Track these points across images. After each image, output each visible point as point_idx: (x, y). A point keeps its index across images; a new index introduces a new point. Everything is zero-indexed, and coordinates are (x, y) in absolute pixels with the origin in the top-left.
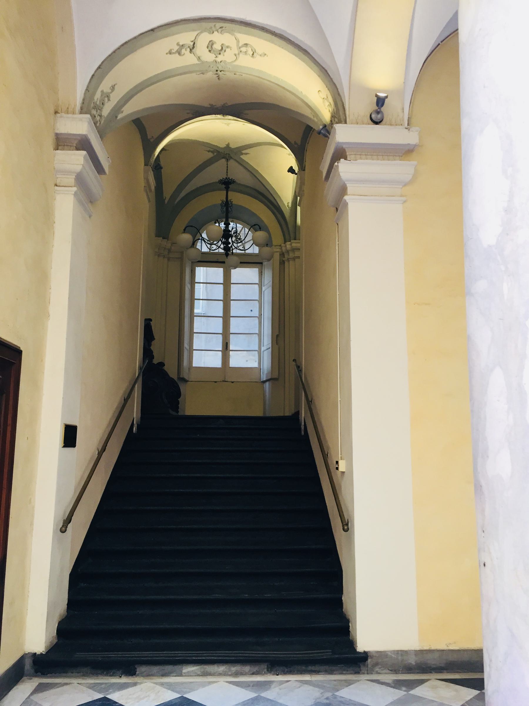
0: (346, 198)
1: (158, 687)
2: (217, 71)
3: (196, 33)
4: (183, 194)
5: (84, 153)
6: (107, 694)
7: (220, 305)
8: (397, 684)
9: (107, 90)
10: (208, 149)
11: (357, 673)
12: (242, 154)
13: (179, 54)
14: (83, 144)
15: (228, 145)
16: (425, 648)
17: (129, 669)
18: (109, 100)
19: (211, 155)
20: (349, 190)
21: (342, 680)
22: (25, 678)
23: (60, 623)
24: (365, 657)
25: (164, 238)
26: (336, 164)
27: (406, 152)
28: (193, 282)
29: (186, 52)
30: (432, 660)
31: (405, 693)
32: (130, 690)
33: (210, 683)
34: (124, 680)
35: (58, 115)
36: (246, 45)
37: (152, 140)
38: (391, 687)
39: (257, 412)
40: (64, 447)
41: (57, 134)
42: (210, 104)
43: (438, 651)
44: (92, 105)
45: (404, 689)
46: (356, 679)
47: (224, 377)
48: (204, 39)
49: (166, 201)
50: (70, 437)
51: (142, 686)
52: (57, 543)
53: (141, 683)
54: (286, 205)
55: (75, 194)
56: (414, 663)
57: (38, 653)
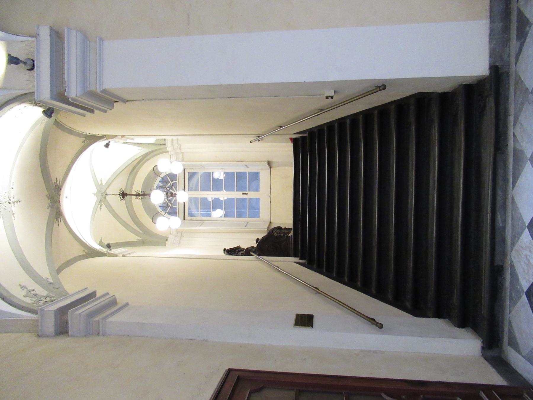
0: (99, 91)
1: (516, 247)
2: (9, 203)
4: (135, 227)
8: (522, 35)
10: (99, 208)
11: (508, 74)
12: (102, 184)
16: (488, 14)
17: (497, 272)
18: (33, 290)
19: (103, 207)
21: (515, 89)
24: (494, 69)
25: (167, 240)
26: (70, 100)
27: (57, 37)
32: (519, 271)
34: (508, 276)
38: (524, 41)
40: (312, 327)
42: (48, 208)
46: (514, 75)
49: (140, 239)
50: (305, 321)
53: (512, 261)
54: (140, 151)
57: (482, 345)
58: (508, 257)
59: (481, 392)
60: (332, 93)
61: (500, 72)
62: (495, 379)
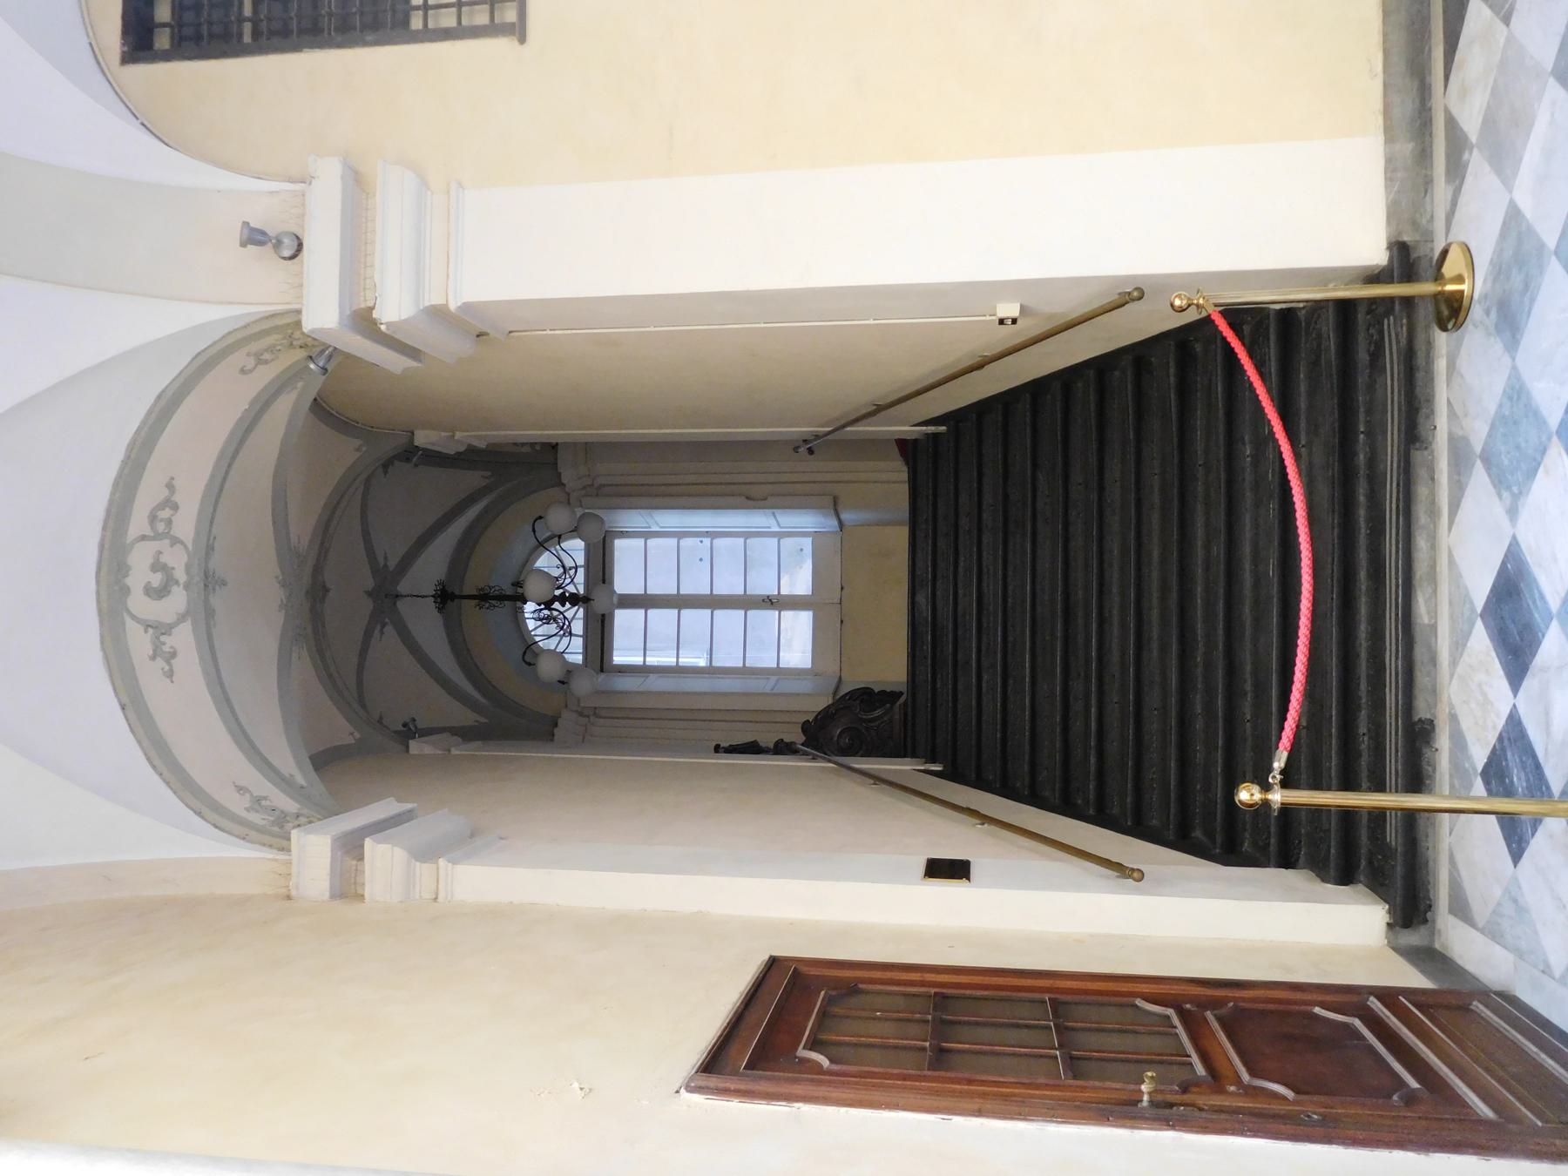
0: (453, 306)
1: (1460, 670)
3: (128, 620)
5: (368, 842)
6: (1475, 769)
7: (687, 614)
8: (1456, 170)
9: (246, 801)
12: (386, 566)
13: (174, 654)
14: (351, 846)
15: (369, 594)
18: (265, 798)
20: (437, 300)
22: (1437, 946)
23: (1324, 880)
26: (383, 327)
27: (357, 185)
28: (644, 670)
29: (169, 642)
30: (1405, 107)
31: (1475, 151)
32: (1466, 724)
33: (1452, 562)
34: (1443, 741)
35: (293, 893)
36: (153, 518)
37: (357, 735)
39: (899, 538)
40: (968, 879)
41: (333, 896)
43: (1385, 95)
44: (276, 829)
45: (1466, 156)
47: (833, 609)
48: (138, 603)
49: (483, 720)
50: (941, 869)
51: (1456, 701)
52: (1162, 886)
53: (1451, 706)
55: (454, 862)
56: (1411, 146)
58: (1445, 698)
59: (1372, 998)
60: (1015, 313)
61: (1414, 256)
62: (1411, 977)
